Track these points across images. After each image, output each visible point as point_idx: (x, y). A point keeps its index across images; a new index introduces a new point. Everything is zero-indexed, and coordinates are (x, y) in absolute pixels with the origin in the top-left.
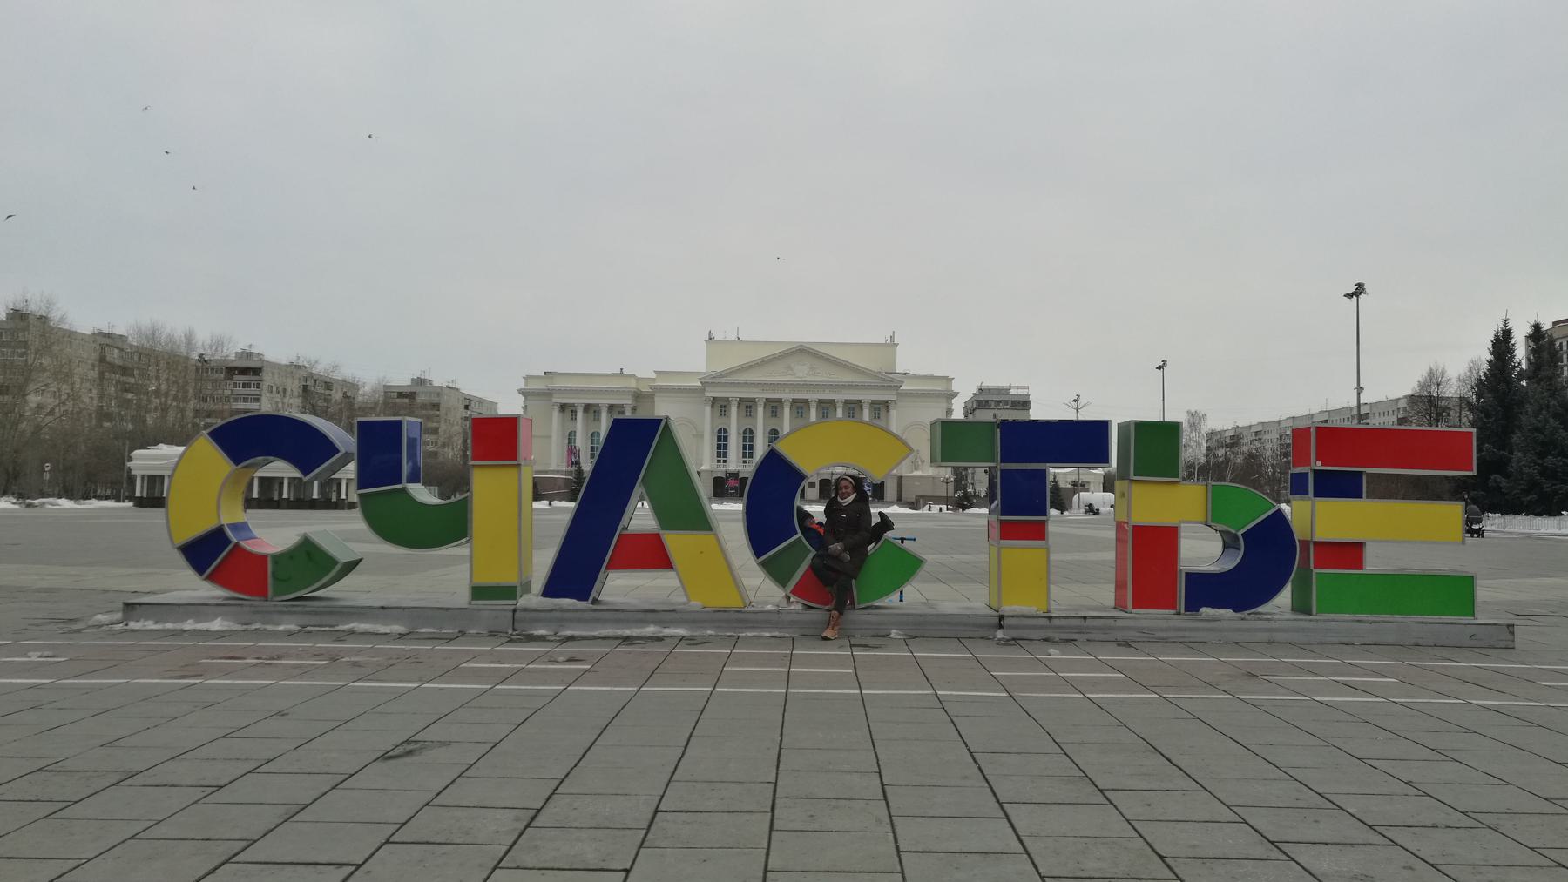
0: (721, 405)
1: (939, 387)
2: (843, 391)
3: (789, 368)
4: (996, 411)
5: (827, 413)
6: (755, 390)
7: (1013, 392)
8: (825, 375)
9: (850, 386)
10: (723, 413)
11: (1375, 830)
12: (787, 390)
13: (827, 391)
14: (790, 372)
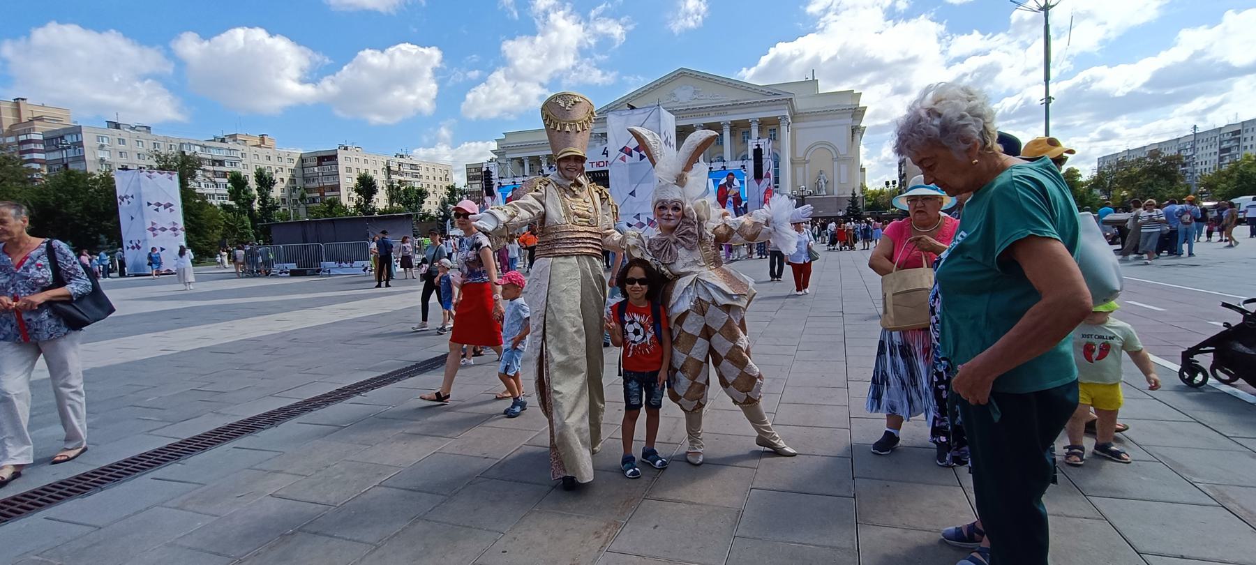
1: (849, 103)
2: (729, 112)
3: (673, 95)
5: (774, 135)
7: (825, 87)
9: (735, 106)
11: (170, 422)
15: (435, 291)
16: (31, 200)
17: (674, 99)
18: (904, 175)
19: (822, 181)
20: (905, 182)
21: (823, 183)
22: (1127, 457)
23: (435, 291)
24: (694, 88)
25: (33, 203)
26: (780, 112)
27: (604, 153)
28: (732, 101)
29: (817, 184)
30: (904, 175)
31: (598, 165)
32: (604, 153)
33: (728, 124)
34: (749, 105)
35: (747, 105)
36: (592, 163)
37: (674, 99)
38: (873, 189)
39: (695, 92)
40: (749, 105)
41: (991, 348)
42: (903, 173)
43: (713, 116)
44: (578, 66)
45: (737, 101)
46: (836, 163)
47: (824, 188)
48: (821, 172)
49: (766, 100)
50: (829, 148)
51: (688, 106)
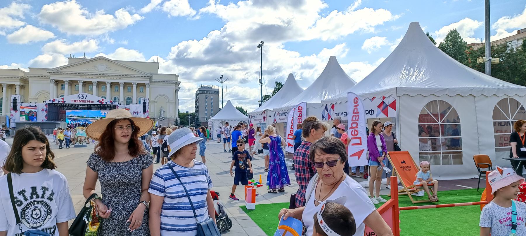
0: (57, 82)
2: (123, 79)
4: (207, 95)
6: (79, 77)
8: (114, 71)
9: (126, 76)
10: (63, 88)
12: (95, 77)
13: (115, 78)
14: (96, 69)
15: (240, 182)
16: (13, 153)
17: (96, 69)
18: (198, 107)
19: (162, 111)
20: (198, 110)
21: (163, 112)
22: (416, 72)
23: (240, 182)
24: (107, 66)
25: (10, 163)
26: (147, 81)
27: (78, 97)
28: (125, 74)
29: (160, 112)
30: (198, 107)
31: (75, 101)
32: (78, 97)
33: (95, 82)
34: (133, 76)
35: (132, 77)
36: (72, 100)
37: (96, 69)
38: (183, 112)
39: (107, 67)
40: (133, 76)
41: (212, 198)
42: (197, 106)
43: (95, 79)
44: (519, 131)
45: (127, 74)
46: (168, 104)
47: (163, 114)
48: (162, 107)
49: (144, 76)
50: (165, 97)
51: (103, 73)
